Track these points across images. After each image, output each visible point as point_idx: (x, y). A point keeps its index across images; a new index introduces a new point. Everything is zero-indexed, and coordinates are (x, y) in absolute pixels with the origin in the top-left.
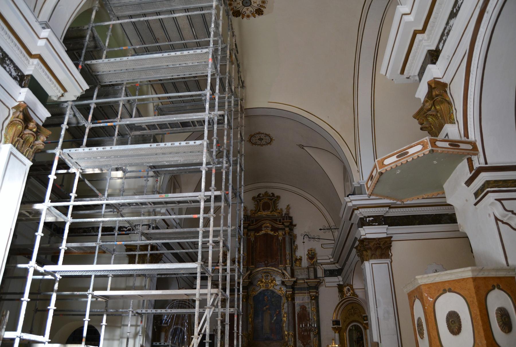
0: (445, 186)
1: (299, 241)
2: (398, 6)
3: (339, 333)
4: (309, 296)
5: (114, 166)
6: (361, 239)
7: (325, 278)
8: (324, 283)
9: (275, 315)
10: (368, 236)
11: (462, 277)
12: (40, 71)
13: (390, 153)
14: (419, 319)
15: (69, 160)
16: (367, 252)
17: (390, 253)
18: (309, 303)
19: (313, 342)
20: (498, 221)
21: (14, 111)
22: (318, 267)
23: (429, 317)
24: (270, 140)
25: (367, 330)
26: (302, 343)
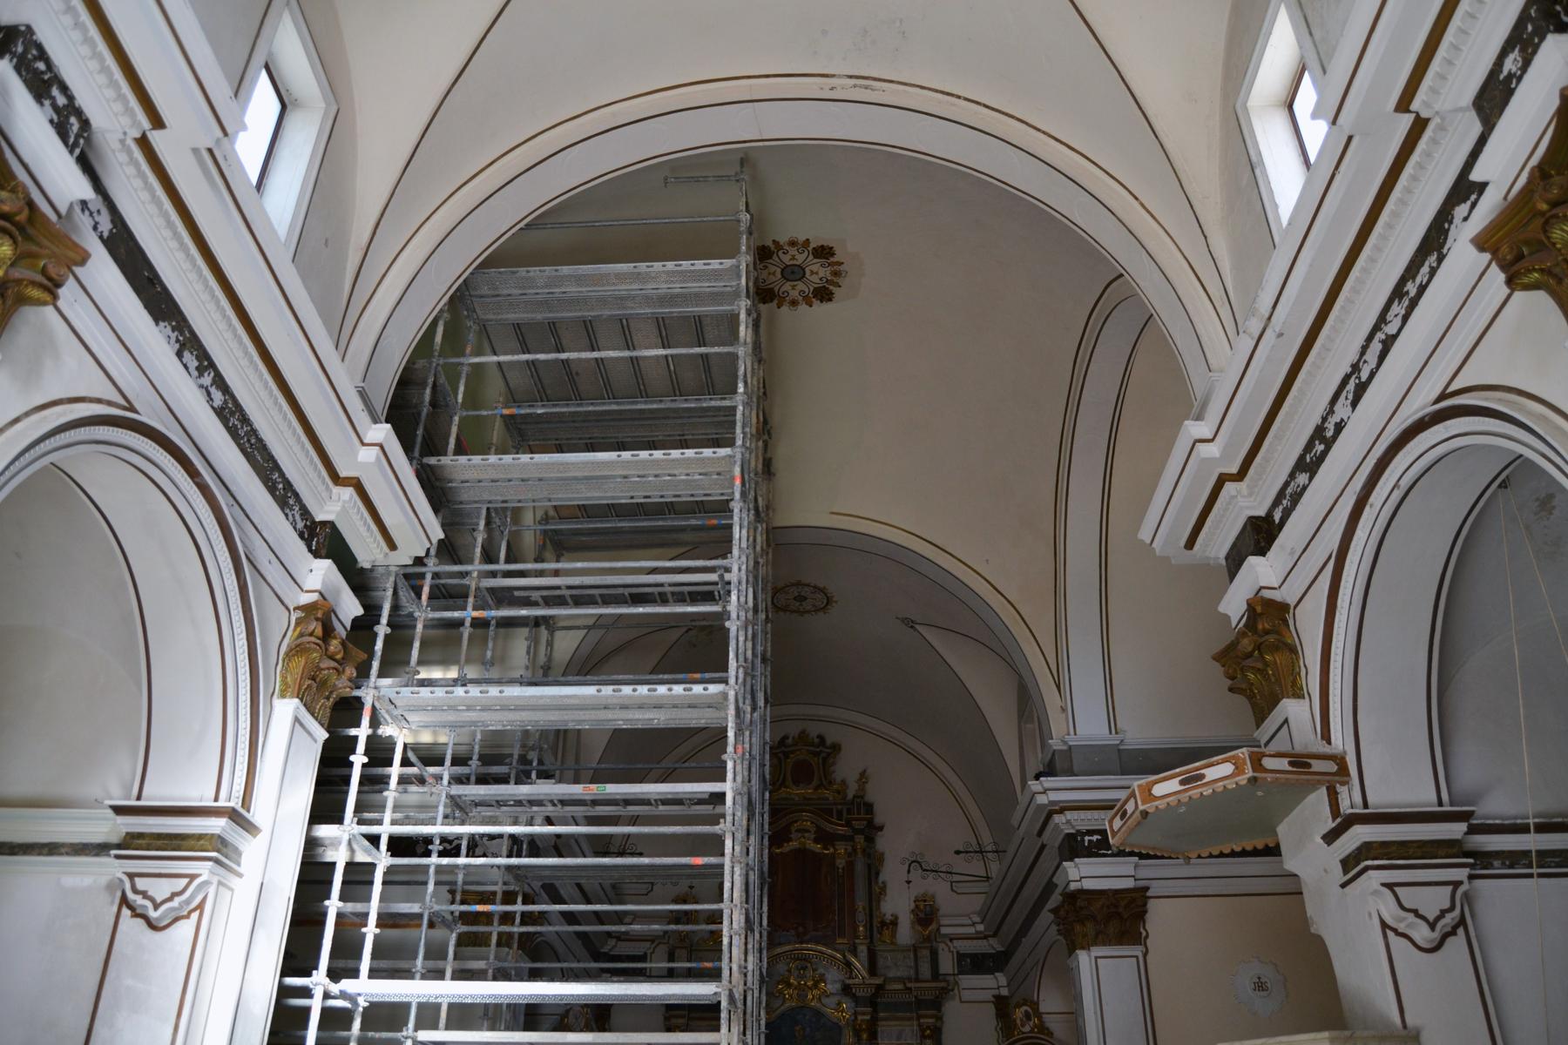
1: (892, 872)
2: (1186, 422)
5: (492, 725)
6: (1067, 890)
8: (956, 991)
10: (1088, 885)
12: (356, 518)
15: (387, 711)
17: (1142, 930)
21: (299, 616)
22: (942, 946)
24: (825, 601)
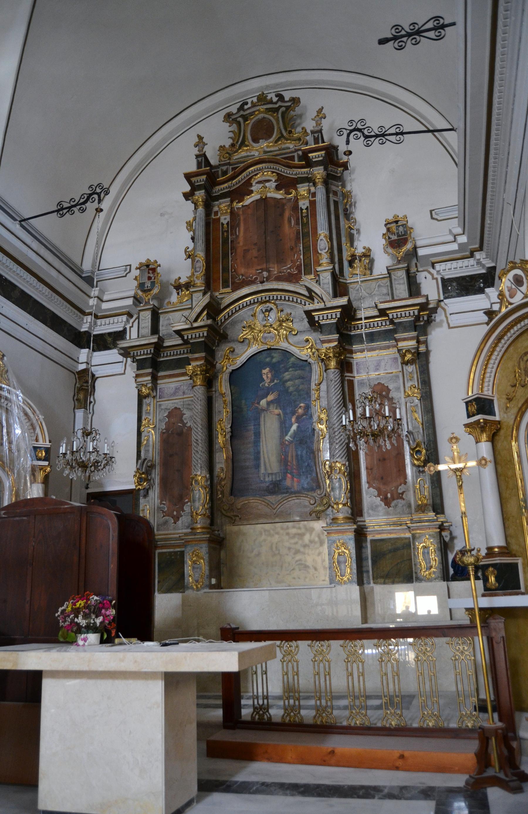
3: (493, 439)
4: (397, 355)
7: (446, 301)
9: (293, 420)
18: (397, 377)
19: (415, 488)
26: (379, 495)
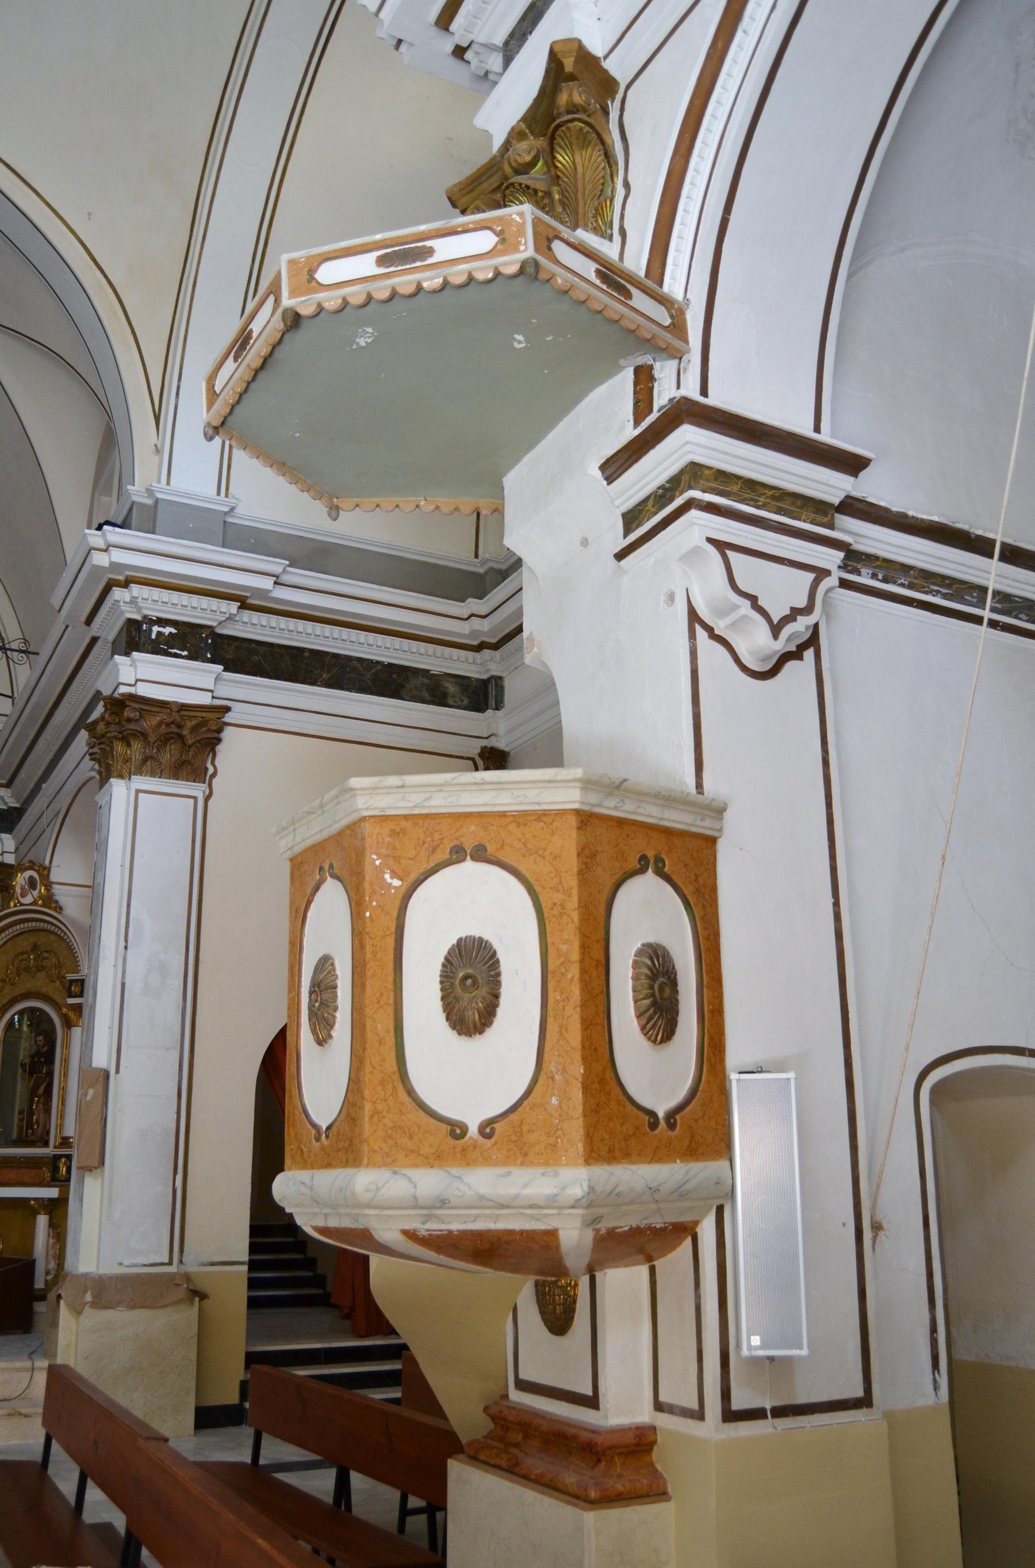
0: (511, 481)
6: (116, 695)
10: (144, 690)
11: (539, 804)
13: (352, 238)
14: (325, 963)
16: (129, 745)
17: (209, 765)
20: (698, 627)
23: (374, 954)
25: (74, 1029)
